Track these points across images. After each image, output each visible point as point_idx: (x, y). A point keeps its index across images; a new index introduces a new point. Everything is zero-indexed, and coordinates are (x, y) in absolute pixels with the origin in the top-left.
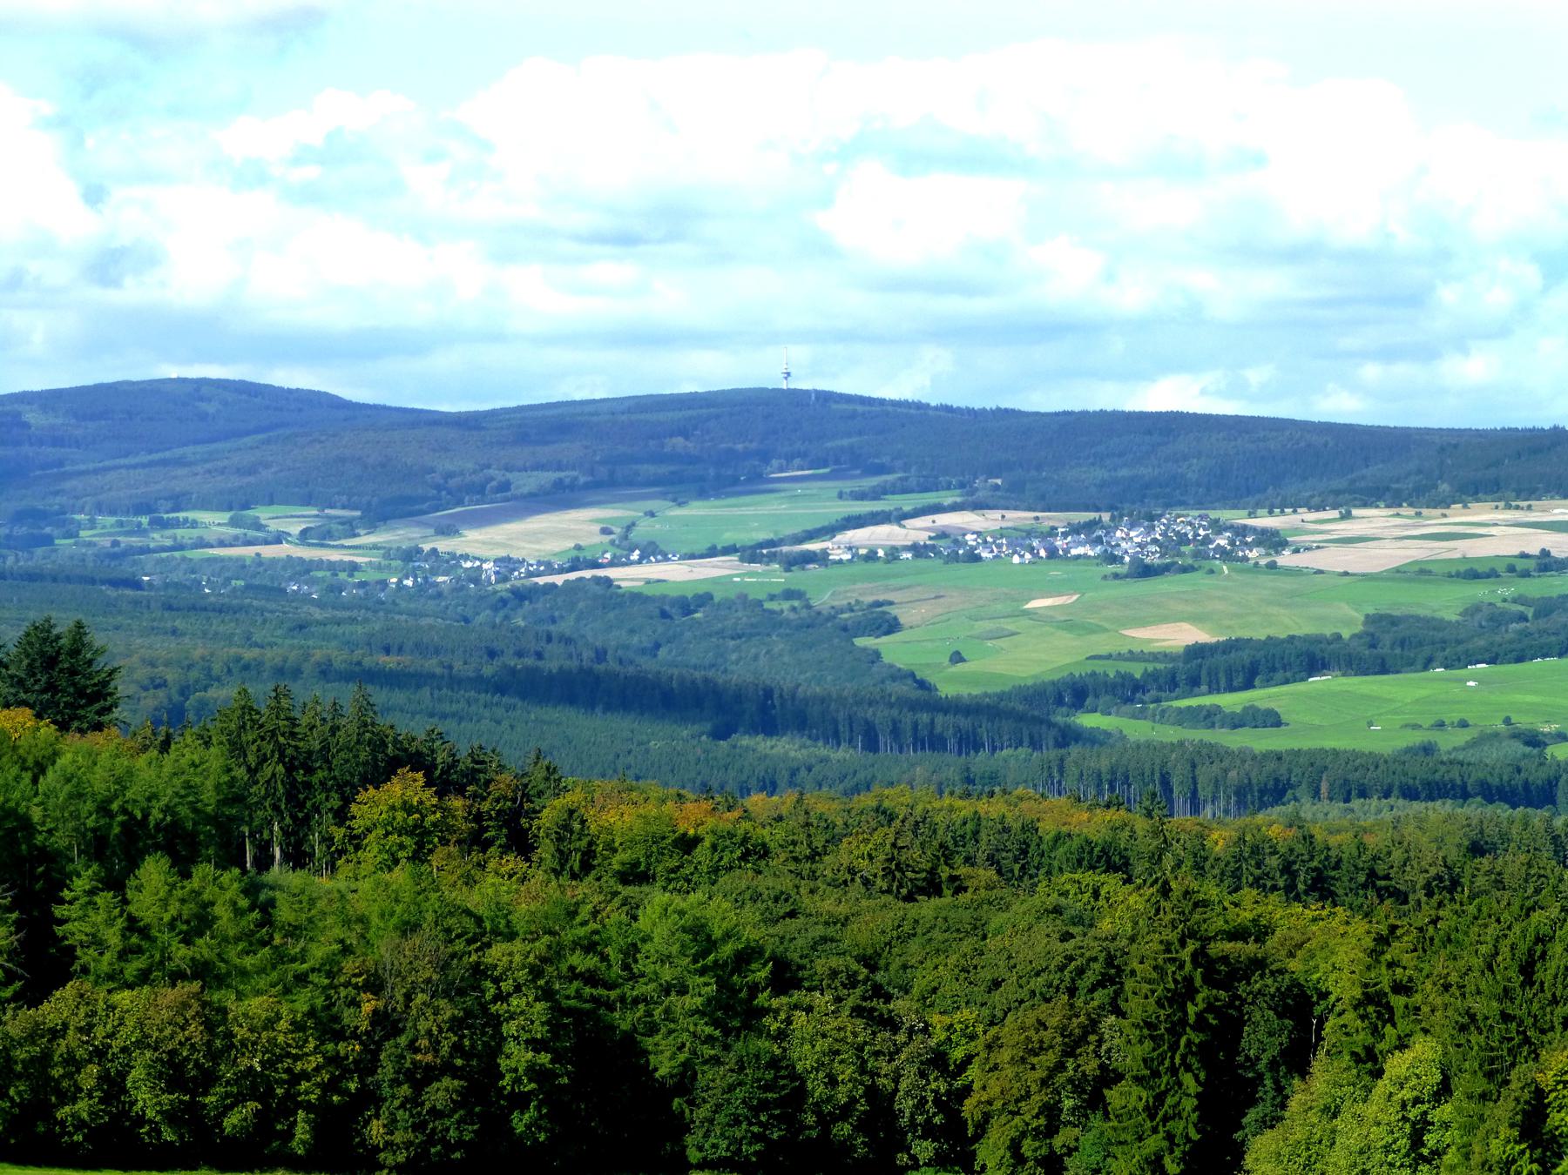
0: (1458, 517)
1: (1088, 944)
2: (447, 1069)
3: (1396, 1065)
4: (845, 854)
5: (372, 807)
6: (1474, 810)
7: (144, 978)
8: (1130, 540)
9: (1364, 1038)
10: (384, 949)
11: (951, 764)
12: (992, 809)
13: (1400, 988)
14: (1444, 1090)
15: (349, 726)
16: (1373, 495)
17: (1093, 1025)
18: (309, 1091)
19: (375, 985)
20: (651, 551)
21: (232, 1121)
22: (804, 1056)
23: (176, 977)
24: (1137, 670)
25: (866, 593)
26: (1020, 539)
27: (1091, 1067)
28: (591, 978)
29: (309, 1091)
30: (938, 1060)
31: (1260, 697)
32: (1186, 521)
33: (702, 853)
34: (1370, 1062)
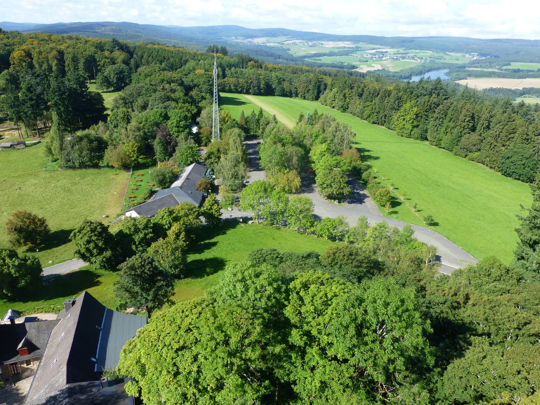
0: (338, 43)
1: (309, 79)
2: (256, 86)
3: (333, 90)
4: (288, 70)
5: (250, 64)
6: (337, 69)
7: (232, 77)
8: (310, 43)
9: (331, 88)
10: (251, 76)
11: (294, 63)
12: (299, 67)
13: (334, 84)
14: (337, 92)
15: (247, 56)
16: (331, 40)
17: (308, 86)
18: (245, 87)
19: (251, 79)
20: (270, 42)
21: (239, 90)
22: (285, 87)
23: (235, 77)
24: (310, 55)
25: (288, 47)
26: (301, 43)
27: (308, 89)
28: (268, 79)
29: (245, 87)
30: (296, 88)
31: (320, 58)
32: (315, 42)
33: (276, 69)
34: (331, 90)
